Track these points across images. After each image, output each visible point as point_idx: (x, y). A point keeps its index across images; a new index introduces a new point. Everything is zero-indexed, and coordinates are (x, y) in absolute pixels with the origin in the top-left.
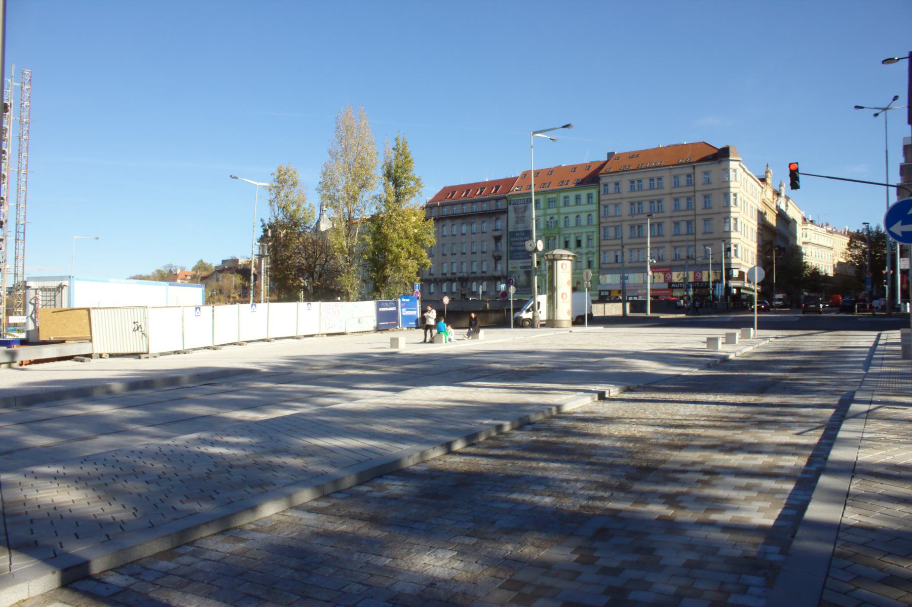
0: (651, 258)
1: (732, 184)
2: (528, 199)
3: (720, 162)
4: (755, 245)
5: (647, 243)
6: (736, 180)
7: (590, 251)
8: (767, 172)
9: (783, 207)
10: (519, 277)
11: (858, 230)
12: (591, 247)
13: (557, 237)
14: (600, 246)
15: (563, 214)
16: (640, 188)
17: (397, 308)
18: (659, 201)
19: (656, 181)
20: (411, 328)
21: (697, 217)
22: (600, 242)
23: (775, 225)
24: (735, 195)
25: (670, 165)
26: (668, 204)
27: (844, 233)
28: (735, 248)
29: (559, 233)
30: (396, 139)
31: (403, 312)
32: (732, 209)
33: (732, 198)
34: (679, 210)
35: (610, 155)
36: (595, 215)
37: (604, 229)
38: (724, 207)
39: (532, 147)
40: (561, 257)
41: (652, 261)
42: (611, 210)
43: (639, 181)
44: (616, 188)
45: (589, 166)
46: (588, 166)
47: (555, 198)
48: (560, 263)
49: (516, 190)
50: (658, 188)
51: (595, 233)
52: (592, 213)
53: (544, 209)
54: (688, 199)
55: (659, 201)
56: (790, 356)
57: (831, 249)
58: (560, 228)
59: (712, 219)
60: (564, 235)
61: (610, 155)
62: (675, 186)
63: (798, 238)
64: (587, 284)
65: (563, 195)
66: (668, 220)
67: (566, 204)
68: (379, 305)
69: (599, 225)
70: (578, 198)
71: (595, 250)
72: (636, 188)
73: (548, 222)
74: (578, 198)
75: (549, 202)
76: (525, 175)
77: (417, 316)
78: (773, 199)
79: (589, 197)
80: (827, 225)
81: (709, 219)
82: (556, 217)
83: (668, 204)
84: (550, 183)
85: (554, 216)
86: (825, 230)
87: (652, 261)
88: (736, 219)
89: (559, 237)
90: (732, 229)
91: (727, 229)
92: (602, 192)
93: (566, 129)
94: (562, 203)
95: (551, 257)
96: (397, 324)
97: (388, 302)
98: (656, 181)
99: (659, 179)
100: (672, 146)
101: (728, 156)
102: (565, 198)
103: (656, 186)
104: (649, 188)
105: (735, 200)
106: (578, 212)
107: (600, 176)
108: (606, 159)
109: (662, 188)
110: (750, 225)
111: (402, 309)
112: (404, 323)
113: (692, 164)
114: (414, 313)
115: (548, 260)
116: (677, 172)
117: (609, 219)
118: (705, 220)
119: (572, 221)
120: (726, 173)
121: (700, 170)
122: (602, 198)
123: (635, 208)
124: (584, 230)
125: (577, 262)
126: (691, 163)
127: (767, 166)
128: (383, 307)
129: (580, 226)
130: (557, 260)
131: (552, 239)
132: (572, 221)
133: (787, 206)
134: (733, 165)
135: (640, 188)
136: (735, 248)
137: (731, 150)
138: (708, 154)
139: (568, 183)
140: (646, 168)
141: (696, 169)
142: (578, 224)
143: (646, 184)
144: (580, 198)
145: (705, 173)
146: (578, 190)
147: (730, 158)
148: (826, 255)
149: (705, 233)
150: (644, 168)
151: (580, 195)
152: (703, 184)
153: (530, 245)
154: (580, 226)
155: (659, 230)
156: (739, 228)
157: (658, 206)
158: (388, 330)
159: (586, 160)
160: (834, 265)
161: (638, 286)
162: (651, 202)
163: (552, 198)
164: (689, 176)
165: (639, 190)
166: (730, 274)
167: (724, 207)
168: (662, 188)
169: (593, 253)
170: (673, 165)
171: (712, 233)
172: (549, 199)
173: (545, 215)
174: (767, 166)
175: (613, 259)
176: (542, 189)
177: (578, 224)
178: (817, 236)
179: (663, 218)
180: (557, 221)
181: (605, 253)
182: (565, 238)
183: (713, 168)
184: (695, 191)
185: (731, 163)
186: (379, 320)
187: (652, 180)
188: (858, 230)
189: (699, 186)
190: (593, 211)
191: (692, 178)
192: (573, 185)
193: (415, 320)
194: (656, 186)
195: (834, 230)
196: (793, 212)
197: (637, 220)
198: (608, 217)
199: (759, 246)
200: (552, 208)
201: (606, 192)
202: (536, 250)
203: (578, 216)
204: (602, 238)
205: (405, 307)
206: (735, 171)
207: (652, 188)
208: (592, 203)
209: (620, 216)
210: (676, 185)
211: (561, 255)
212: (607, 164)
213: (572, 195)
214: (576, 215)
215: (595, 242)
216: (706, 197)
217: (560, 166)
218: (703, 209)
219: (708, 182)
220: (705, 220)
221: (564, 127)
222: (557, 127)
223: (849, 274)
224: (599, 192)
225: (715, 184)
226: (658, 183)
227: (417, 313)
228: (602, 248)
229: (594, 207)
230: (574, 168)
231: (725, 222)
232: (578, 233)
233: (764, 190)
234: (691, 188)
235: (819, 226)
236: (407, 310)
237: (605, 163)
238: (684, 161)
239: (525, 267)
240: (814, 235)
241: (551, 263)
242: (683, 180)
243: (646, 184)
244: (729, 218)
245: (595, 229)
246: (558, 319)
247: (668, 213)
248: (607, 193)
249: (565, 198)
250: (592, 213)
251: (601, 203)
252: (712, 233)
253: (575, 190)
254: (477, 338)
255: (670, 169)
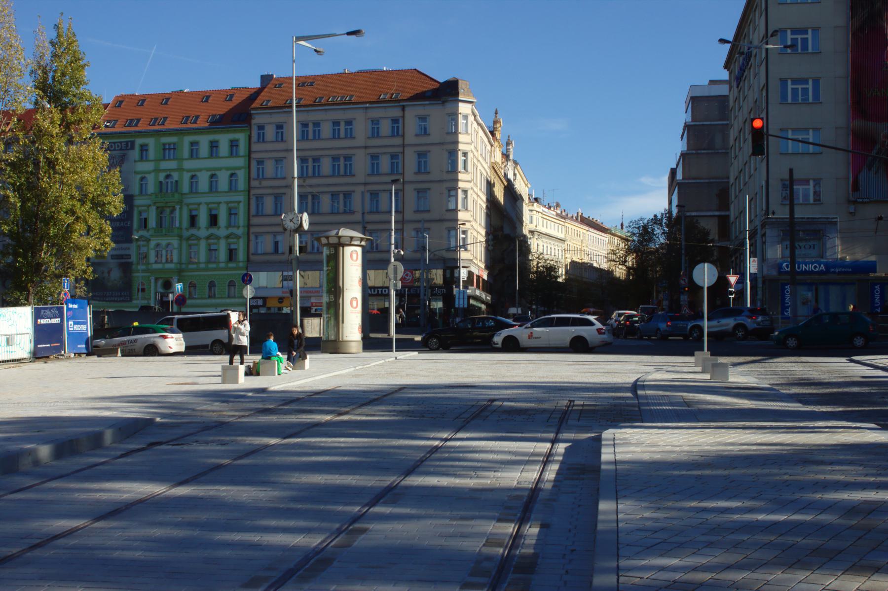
0: (396, 248)
1: (461, 138)
2: (127, 142)
3: (444, 102)
4: (483, 232)
5: (390, 222)
6: (467, 132)
7: (232, 234)
8: (495, 122)
9: (511, 176)
10: (109, 273)
11: (655, 216)
12: (234, 227)
13: (178, 207)
14: (249, 226)
15: (189, 171)
16: (317, 136)
17: (62, 320)
18: (348, 158)
19: (342, 127)
20: (80, 354)
21: (407, 187)
22: (249, 220)
23: (503, 203)
24: (465, 154)
25: (366, 103)
26: (361, 164)
27: (577, 219)
28: (464, 236)
29: (180, 202)
30: (57, 27)
31: (72, 326)
32: (461, 176)
33: (461, 158)
34: (378, 174)
35: (266, 79)
36: (241, 175)
37: (257, 198)
38: (448, 172)
39: (293, 61)
40: (350, 242)
41: (399, 252)
42: (269, 168)
43: (317, 124)
44: (278, 133)
45: (232, 96)
46: (229, 95)
47: (174, 144)
48: (348, 250)
49: (106, 126)
50: (346, 137)
51: (241, 205)
52: (237, 172)
53: (156, 160)
54: (394, 156)
55: (348, 158)
56: (826, 388)
57: (563, 241)
58: (182, 194)
59: (429, 189)
60: (188, 205)
61: (266, 79)
62: (373, 137)
63: (524, 224)
64: (395, 285)
65: (188, 139)
66: (361, 188)
67: (194, 154)
68: (37, 315)
69: (249, 192)
70: (214, 145)
71: (240, 231)
72: (311, 136)
73: (161, 182)
74: (214, 145)
75: (164, 149)
76: (121, 102)
77: (86, 334)
78: (502, 163)
79: (234, 144)
80: (558, 205)
81: (425, 190)
82: (175, 176)
83: (361, 164)
84: (165, 119)
85: (172, 173)
86: (555, 213)
87: (399, 252)
88: (465, 192)
89: (181, 209)
90: (460, 207)
91: (451, 206)
92: (254, 137)
93: (353, 37)
94: (186, 153)
95: (333, 240)
96: (62, 347)
97: (50, 309)
98: (342, 127)
99: (349, 123)
100: (366, 72)
101: (457, 94)
102: (192, 144)
103: (342, 134)
104: (390, 134)
105: (465, 162)
106: (195, 170)
107: (252, 112)
108: (258, 85)
109: (352, 138)
110: (479, 201)
111: (68, 321)
112: (73, 345)
113: (400, 103)
114: (83, 328)
115: (329, 245)
116: (375, 113)
117: (265, 183)
118: (419, 191)
119: (203, 183)
120: (452, 119)
121: (412, 114)
122: (254, 147)
123: (307, 167)
124: (223, 199)
125: (210, 250)
126: (400, 101)
127: (496, 113)
128: (42, 318)
129: (217, 192)
130: (343, 245)
131: (168, 210)
132: (203, 183)
133: (515, 175)
134: (464, 109)
135: (317, 136)
136: (464, 236)
137: (461, 85)
138: (424, 89)
139: (164, 121)
140: (329, 105)
141: (406, 112)
142: (213, 187)
143: (326, 130)
144: (217, 147)
145: (419, 118)
146: (215, 133)
147: (460, 98)
148: (549, 248)
149: (417, 211)
150: (325, 105)
151: (217, 142)
152: (417, 135)
153: (291, 221)
154: (217, 192)
155: (258, 206)
156: (470, 207)
157: (314, 167)
158: (48, 357)
159: (226, 85)
160: (566, 266)
161: (310, 292)
162: (335, 159)
163: (170, 144)
164: (395, 121)
165: (314, 138)
166: (456, 275)
167: (448, 172)
168: (352, 138)
169: (238, 237)
170: (370, 103)
171: (429, 211)
172: (164, 145)
173: (157, 171)
174: (496, 113)
175: (270, 248)
176: (153, 128)
177: (213, 187)
178: (545, 221)
179: (353, 184)
180: (177, 181)
181: (257, 237)
182: (191, 211)
183: (434, 111)
184: (404, 146)
185: (461, 105)
186: (37, 341)
187: (336, 123)
188: (655, 216)
189: (410, 138)
190: (239, 168)
191: (400, 125)
192: (207, 125)
193: (85, 340)
194: (342, 134)
195: (564, 214)
196: (521, 187)
197: (311, 186)
198: (264, 179)
199: (487, 234)
200: (169, 159)
201: (262, 139)
202: (299, 229)
203: (212, 176)
204: (253, 211)
205: (72, 318)
206: (466, 117)
207: (335, 136)
208: (237, 156)
209: (284, 178)
210: (375, 133)
211: (352, 238)
212: (262, 94)
213: (204, 141)
214: (209, 173)
215: (242, 219)
216: (421, 155)
217: (181, 91)
218: (416, 173)
219: (425, 132)
220: (419, 191)
221: (349, 34)
222: (337, 33)
223: (584, 280)
224: (250, 137)
225: (435, 135)
226: (346, 129)
227: (87, 329)
228: (252, 230)
229: (240, 162)
230: (206, 97)
231: (450, 196)
232: (214, 203)
233: (493, 148)
234: (398, 141)
235: (545, 206)
236: (75, 323)
237: (258, 92)
238: (388, 97)
239: (121, 257)
240: (541, 220)
241: (332, 250)
242: (385, 128)
243: (326, 130)
244: (456, 189)
245: (242, 198)
246: (345, 339)
247: (360, 177)
248: (263, 141)
249: (192, 144)
250: (237, 172)
251: (253, 156)
252: (429, 211)
253: (209, 133)
254: (302, 367)
255: (367, 108)
